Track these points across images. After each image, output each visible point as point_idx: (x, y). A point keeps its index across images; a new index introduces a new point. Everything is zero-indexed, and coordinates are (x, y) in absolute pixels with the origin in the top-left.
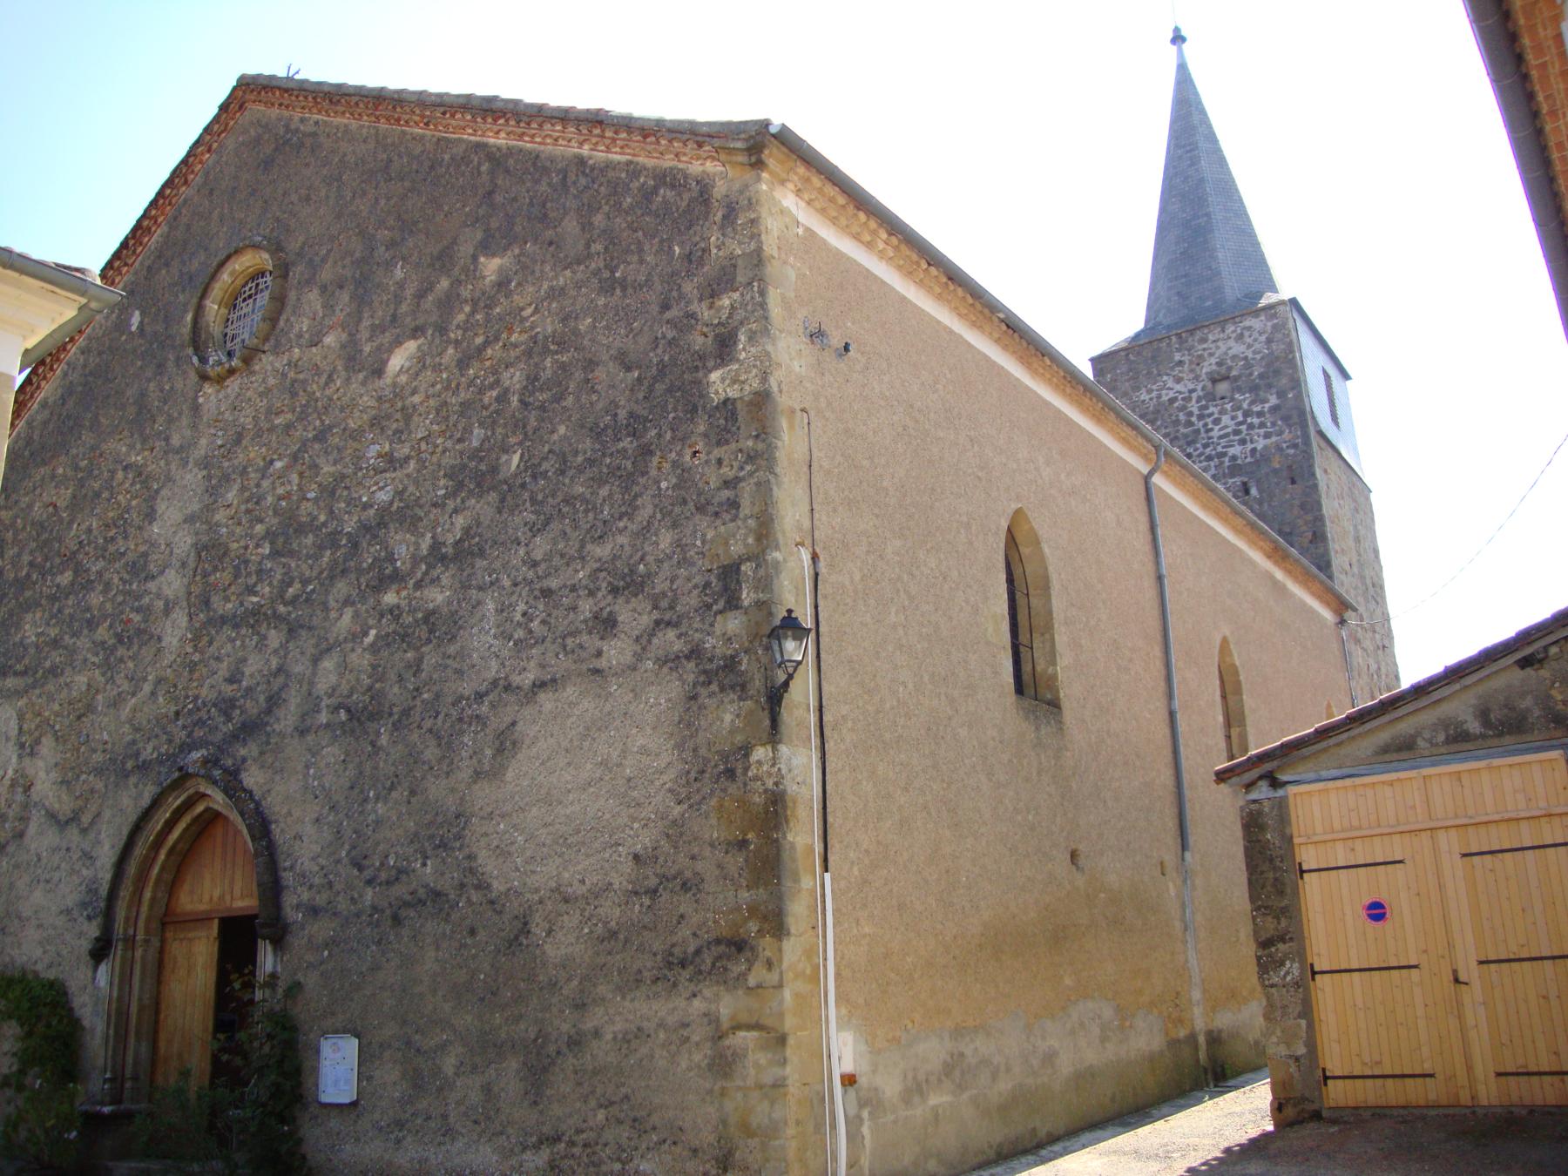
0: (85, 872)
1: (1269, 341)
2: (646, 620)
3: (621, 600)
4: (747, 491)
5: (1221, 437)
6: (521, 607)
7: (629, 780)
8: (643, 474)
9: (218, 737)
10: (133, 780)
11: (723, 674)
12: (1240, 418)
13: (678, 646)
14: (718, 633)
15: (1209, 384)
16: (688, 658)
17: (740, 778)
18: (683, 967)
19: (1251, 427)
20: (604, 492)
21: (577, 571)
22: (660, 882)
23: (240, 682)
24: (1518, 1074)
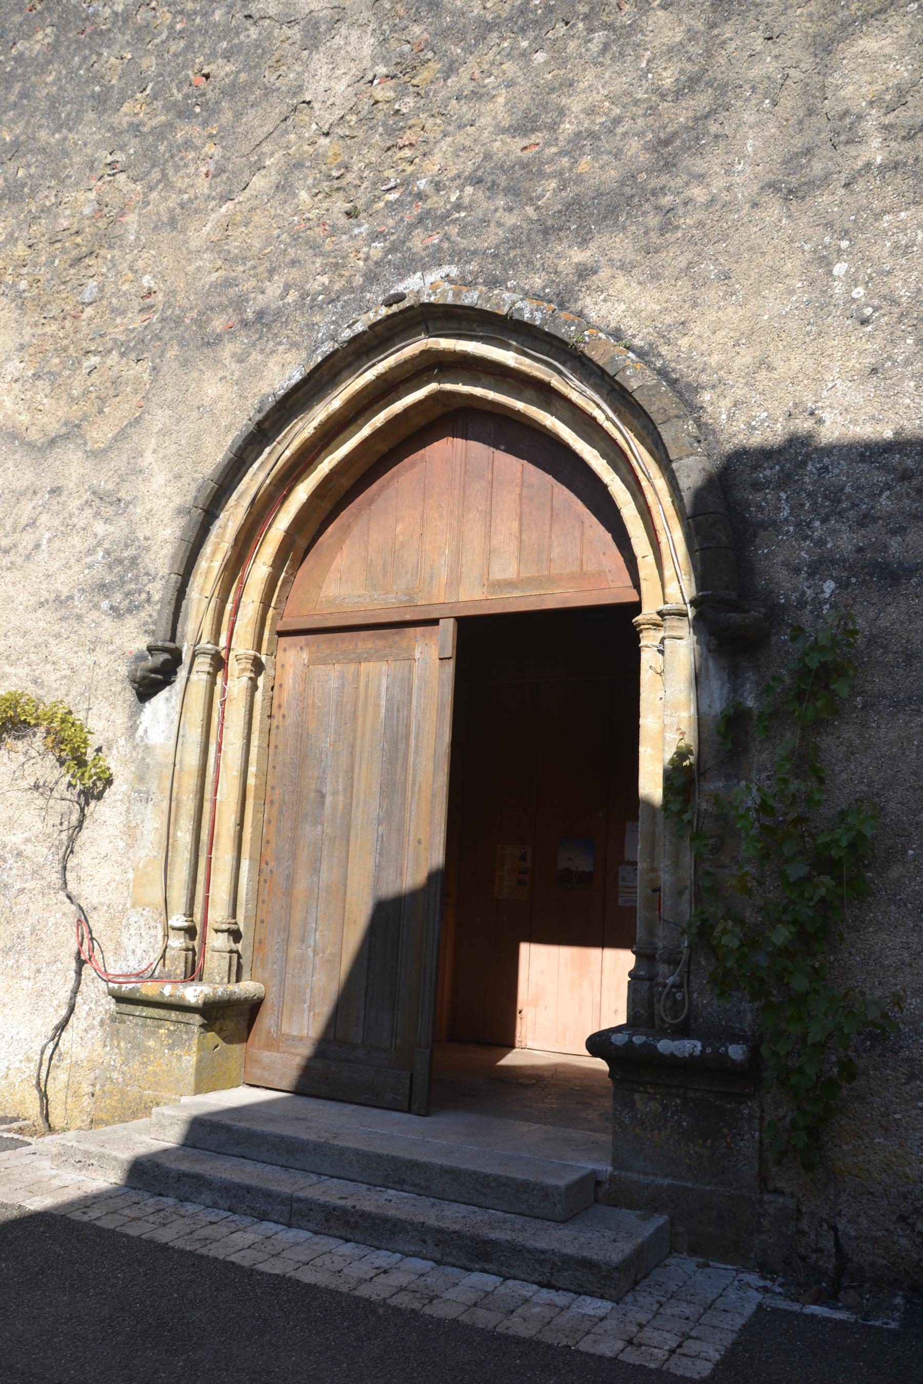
0: (100, 528)
9: (492, 237)
10: (228, 350)
23: (553, 127)
24: (233, 1156)
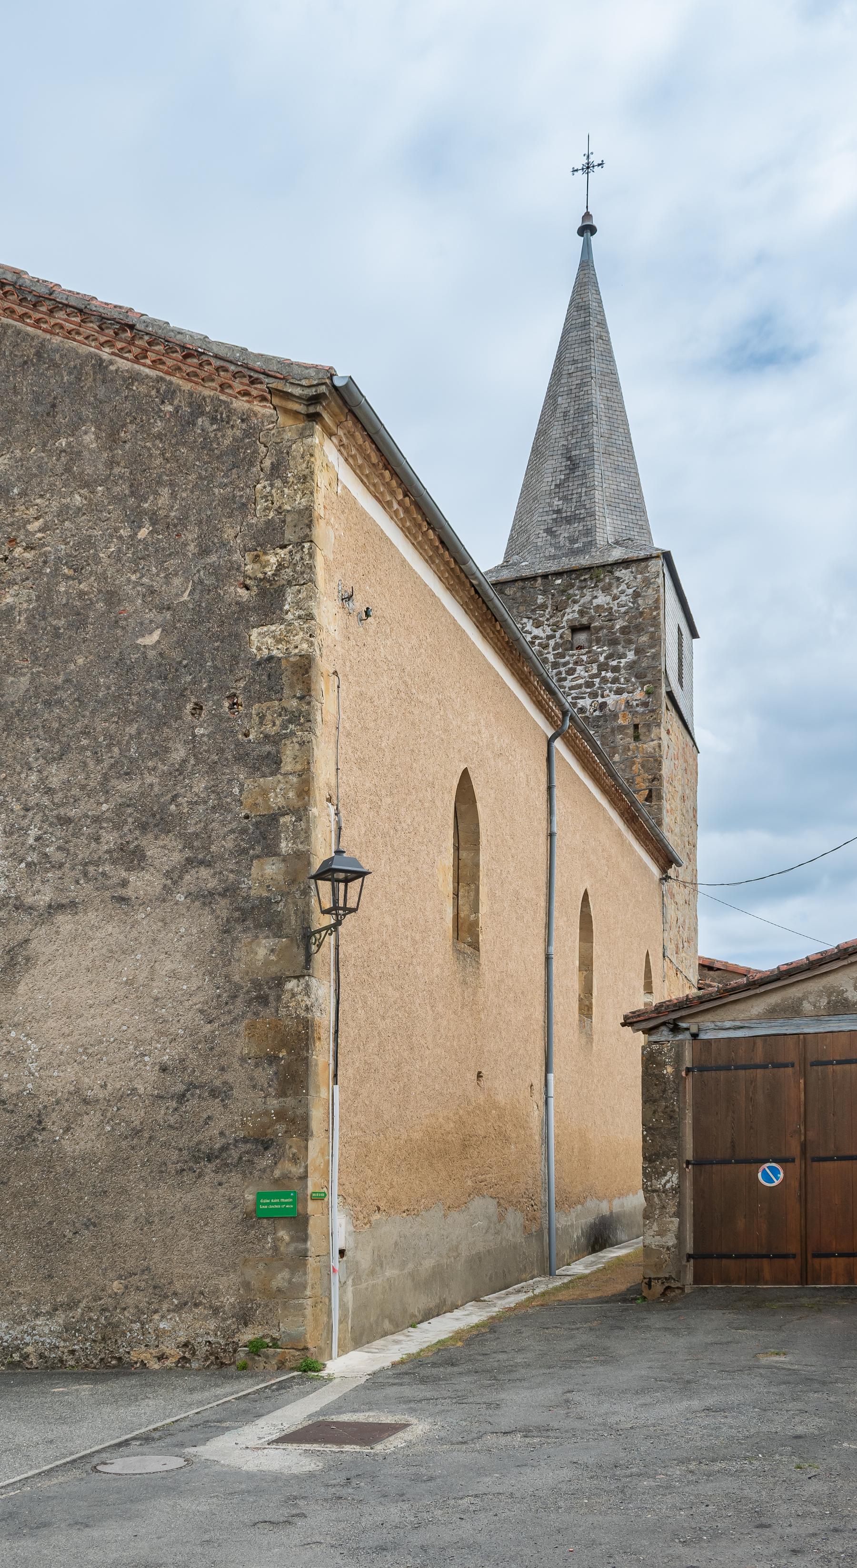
1: (636, 595)
2: (177, 857)
3: (150, 836)
4: (289, 751)
5: (571, 688)
6: (34, 832)
7: (157, 999)
8: (178, 718)
11: (258, 915)
12: (595, 671)
13: (212, 884)
14: (254, 876)
15: (568, 632)
16: (223, 895)
17: (273, 1004)
18: (209, 1161)
19: (604, 680)
20: (132, 729)
21: (100, 804)
22: (184, 1088)
